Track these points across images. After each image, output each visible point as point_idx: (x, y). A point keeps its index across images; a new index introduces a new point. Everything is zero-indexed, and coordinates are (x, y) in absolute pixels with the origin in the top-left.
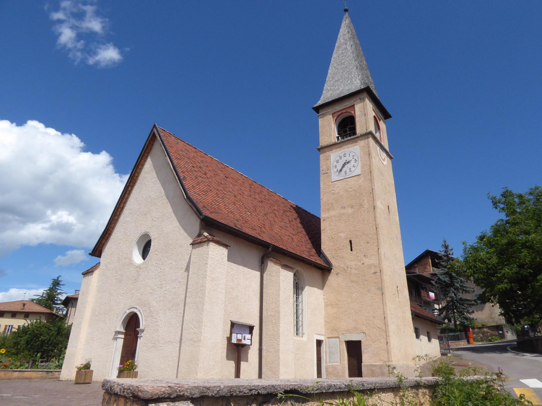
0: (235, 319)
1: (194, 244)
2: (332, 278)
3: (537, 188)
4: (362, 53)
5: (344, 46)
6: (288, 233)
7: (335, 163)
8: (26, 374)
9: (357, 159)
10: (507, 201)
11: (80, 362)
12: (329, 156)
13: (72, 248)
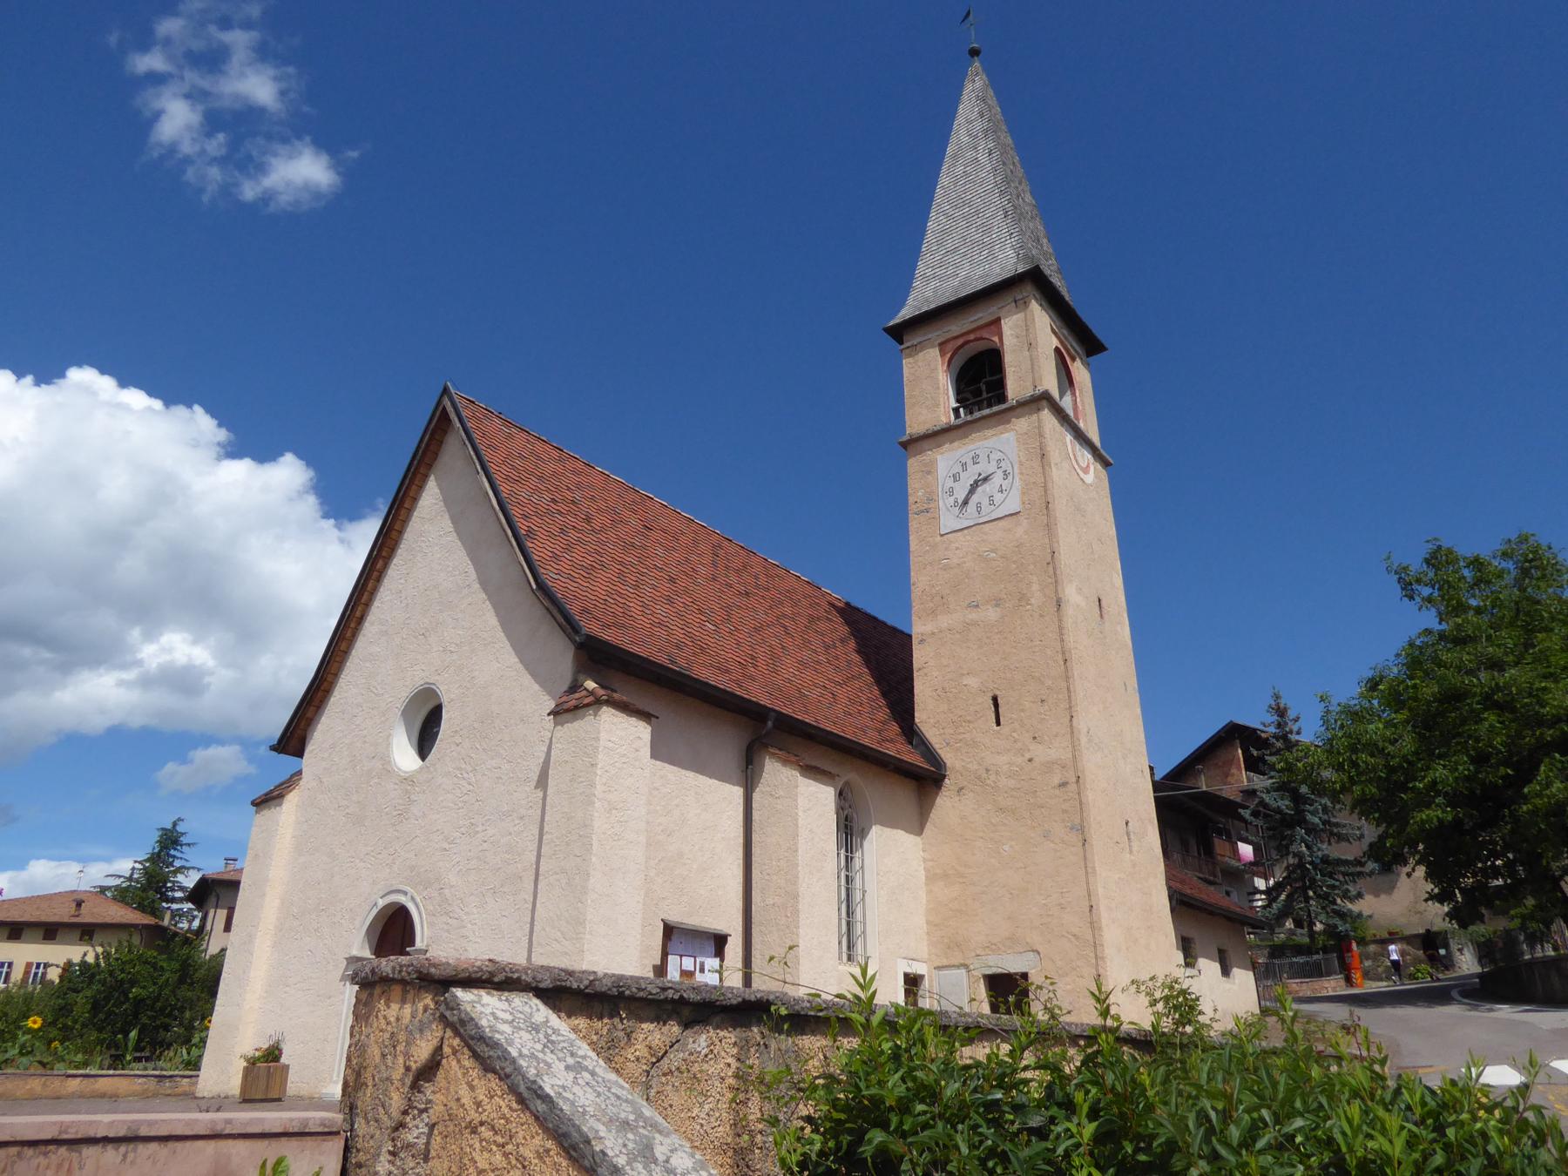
0: (675, 917)
1: (561, 713)
2: (946, 804)
3: (1523, 539)
4: (1020, 172)
5: (970, 154)
6: (821, 681)
7: (950, 483)
8: (103, 1084)
9: (1009, 470)
10: (1441, 577)
11: (250, 1042)
12: (933, 463)
13: (208, 740)
